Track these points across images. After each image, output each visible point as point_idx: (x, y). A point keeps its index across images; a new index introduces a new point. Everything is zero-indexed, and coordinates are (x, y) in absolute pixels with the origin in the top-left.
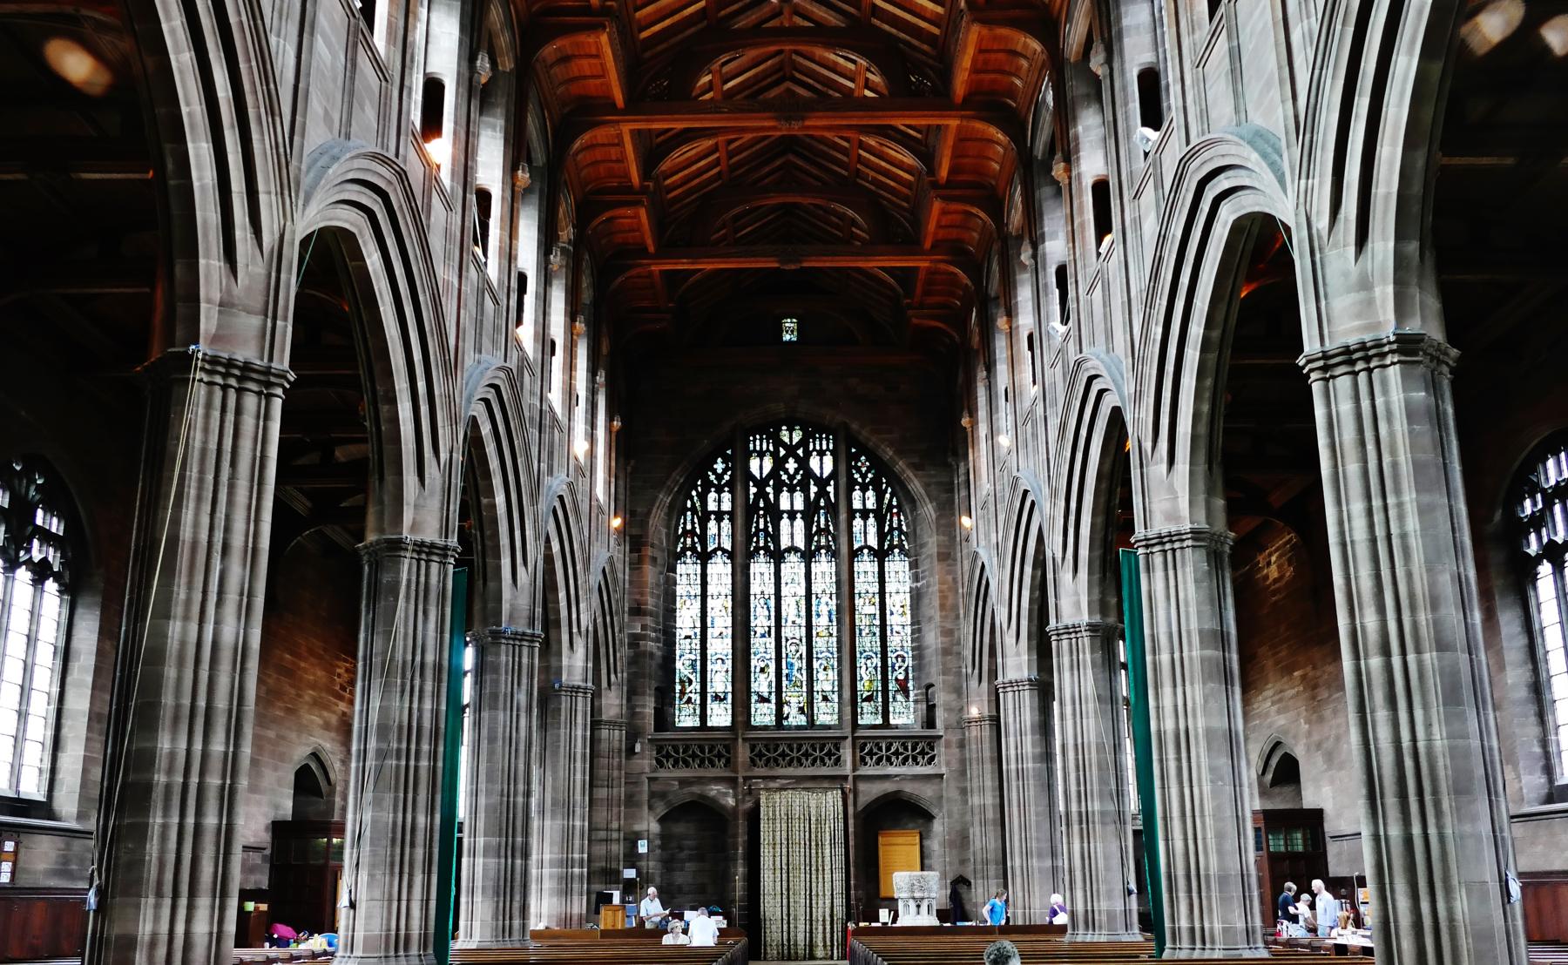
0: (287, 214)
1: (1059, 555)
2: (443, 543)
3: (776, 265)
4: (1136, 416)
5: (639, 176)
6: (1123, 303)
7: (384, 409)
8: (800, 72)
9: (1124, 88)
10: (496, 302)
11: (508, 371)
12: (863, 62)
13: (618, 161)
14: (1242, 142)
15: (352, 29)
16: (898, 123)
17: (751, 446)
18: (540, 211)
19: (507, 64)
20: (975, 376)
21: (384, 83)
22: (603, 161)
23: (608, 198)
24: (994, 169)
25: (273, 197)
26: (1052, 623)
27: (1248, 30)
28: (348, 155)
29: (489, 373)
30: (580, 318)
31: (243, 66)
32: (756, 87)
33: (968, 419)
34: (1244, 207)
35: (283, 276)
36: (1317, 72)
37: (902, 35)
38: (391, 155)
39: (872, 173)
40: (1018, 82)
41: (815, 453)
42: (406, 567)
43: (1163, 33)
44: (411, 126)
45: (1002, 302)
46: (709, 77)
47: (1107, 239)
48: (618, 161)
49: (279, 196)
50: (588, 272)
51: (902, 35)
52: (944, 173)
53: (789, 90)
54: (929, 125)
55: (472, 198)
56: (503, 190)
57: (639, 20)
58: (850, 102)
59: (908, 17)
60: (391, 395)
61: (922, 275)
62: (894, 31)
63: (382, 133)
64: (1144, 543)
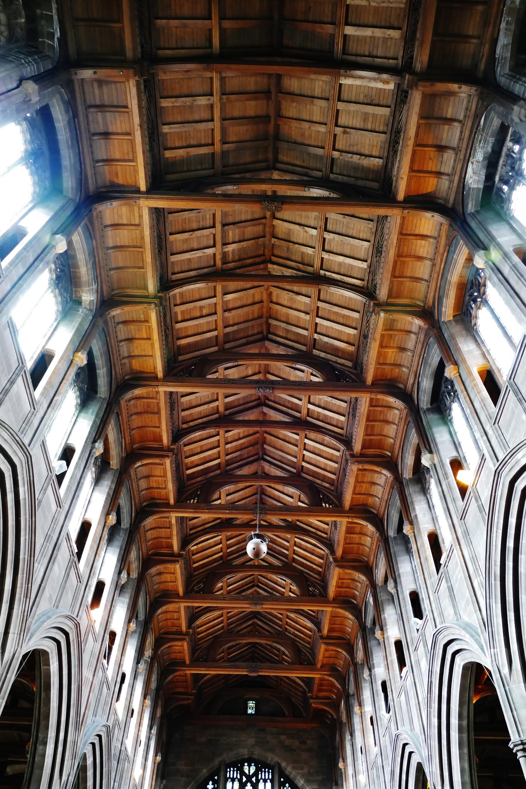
0: (19, 644)
3: (246, 673)
4: (431, 770)
5: (178, 546)
6: (416, 704)
7: (40, 748)
9: (404, 599)
10: (109, 688)
11: (108, 727)
12: (289, 581)
13: (177, 619)
14: (460, 629)
15: (71, 560)
16: (306, 608)
17: (228, 774)
19: (134, 575)
20: (345, 738)
21: (79, 583)
22: (170, 619)
23: (170, 636)
24: (349, 631)
25: (16, 636)
27: (454, 579)
28: (55, 616)
29: (98, 728)
31: (20, 576)
32: (242, 589)
33: (342, 763)
34: (466, 659)
35: (9, 675)
36: (488, 600)
37: (306, 571)
38: (75, 616)
39: (292, 630)
40: (356, 593)
41: (261, 781)
43: (418, 577)
44: (87, 603)
45: (356, 697)
46: (222, 584)
47: (405, 670)
48: (177, 619)
49: (18, 635)
50: (156, 672)
51: (306, 571)
52: (325, 631)
53: (256, 590)
55: (107, 636)
56: (122, 632)
57: (194, 559)
58: (283, 599)
59: (308, 563)
60: (45, 740)
61: (316, 681)
62: (302, 569)
63: (73, 606)
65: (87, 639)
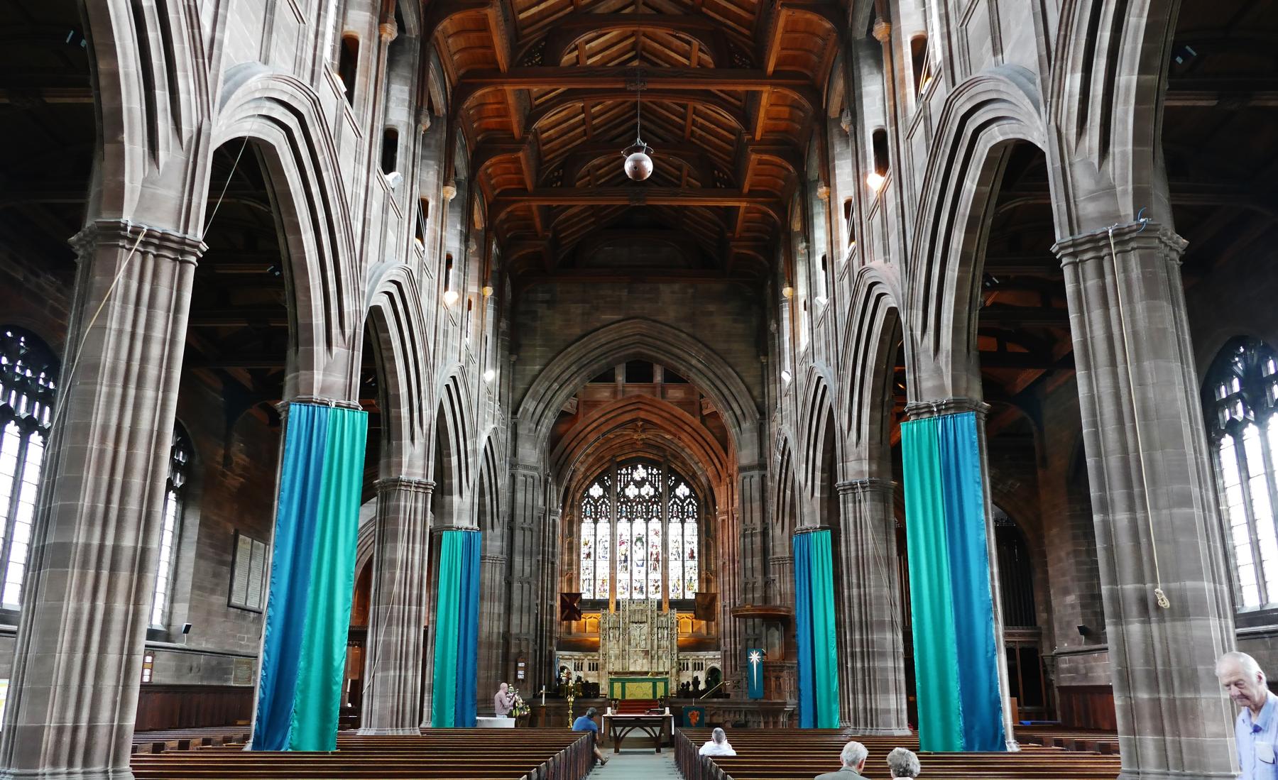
1: (803, 482)
2: (180, 234)
3: (627, 203)
7: (393, 411)
8: (648, 52)
18: (462, 212)
21: (359, 139)
26: (840, 482)
30: (503, 320)
42: (126, 259)
54: (747, 91)
61: (741, 211)
64: (915, 412)
65: (340, 132)
